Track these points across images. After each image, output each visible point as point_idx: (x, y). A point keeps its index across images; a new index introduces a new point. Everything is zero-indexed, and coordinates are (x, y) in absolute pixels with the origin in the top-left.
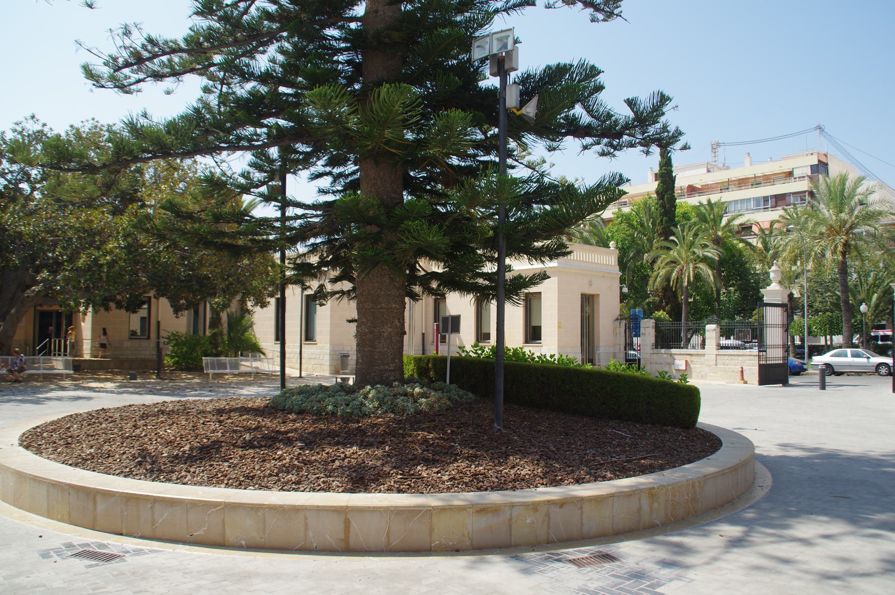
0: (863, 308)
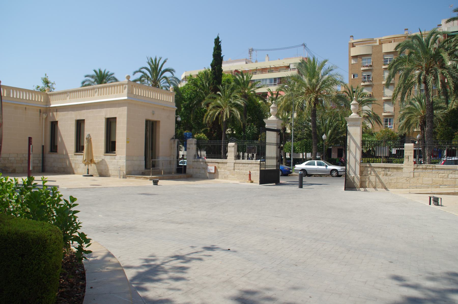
0: (324, 137)
